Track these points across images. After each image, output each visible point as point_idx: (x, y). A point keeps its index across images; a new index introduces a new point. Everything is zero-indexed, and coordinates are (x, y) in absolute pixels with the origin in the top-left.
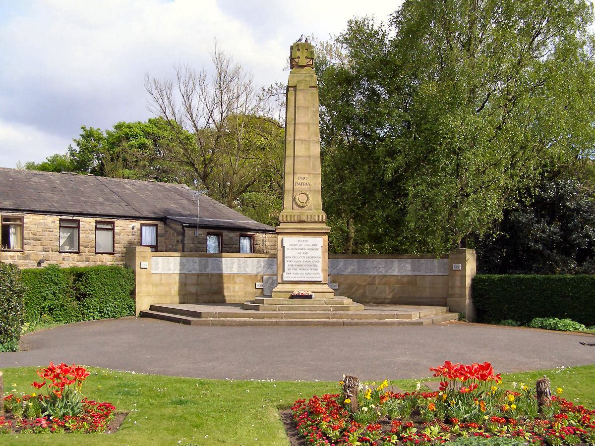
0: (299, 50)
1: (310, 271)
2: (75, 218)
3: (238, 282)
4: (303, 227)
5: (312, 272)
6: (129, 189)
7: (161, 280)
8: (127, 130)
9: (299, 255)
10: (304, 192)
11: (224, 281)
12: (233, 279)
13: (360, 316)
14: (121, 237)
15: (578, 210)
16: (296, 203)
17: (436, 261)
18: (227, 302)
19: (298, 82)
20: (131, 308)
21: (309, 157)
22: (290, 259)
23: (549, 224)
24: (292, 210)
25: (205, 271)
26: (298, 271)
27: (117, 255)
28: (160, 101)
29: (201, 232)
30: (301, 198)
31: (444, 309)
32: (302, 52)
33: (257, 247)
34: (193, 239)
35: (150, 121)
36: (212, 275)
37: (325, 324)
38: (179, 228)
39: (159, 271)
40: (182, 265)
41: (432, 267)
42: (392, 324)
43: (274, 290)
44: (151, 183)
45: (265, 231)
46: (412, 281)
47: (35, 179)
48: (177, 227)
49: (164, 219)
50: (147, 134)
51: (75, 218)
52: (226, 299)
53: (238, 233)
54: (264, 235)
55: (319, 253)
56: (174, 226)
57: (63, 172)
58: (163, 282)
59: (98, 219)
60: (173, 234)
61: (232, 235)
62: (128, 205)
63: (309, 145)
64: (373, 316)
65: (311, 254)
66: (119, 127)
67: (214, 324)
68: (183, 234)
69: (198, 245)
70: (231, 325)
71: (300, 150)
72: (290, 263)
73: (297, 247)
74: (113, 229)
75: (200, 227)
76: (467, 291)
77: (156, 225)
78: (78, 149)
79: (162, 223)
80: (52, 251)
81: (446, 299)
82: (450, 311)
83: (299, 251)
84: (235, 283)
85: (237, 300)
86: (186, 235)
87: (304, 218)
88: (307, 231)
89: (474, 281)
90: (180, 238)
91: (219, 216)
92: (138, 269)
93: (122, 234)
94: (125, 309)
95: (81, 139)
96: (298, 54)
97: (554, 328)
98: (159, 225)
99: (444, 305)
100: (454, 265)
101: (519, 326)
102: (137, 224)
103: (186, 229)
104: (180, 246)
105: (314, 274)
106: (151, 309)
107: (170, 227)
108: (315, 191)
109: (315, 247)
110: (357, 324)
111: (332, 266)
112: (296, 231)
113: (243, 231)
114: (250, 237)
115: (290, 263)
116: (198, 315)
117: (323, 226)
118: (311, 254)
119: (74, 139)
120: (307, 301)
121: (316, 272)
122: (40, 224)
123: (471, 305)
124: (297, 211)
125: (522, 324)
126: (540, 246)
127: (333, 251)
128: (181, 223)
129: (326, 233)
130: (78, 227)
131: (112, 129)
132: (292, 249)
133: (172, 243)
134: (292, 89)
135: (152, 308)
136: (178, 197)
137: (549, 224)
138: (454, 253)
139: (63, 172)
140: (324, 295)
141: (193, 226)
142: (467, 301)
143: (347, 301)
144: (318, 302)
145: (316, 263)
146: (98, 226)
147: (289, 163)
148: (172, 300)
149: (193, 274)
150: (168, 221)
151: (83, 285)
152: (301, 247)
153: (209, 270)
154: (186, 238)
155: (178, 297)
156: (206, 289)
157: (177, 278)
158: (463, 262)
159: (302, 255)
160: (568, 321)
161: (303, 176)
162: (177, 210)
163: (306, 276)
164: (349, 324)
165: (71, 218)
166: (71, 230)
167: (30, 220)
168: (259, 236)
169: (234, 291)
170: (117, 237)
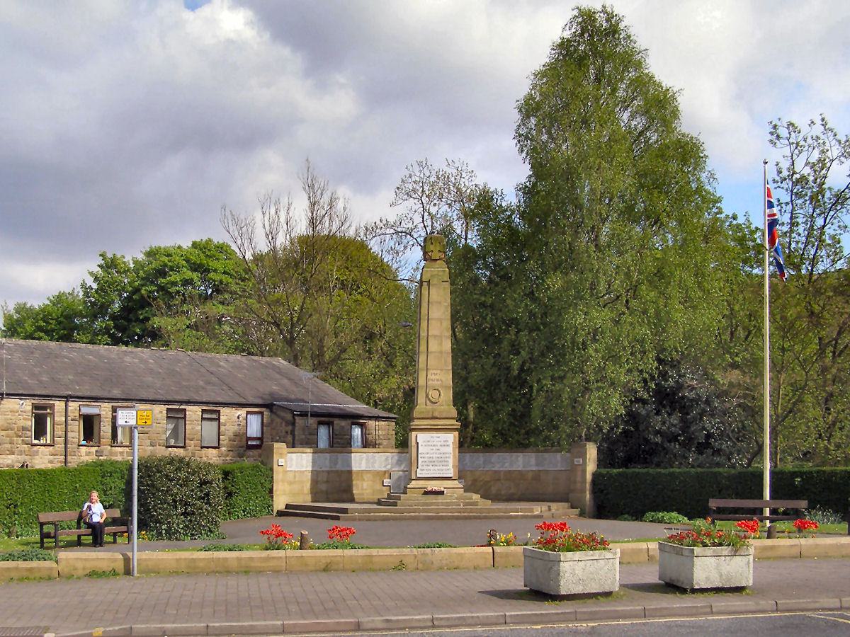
0: (432, 243)
2: (182, 407)
3: (366, 479)
4: (435, 423)
5: (443, 468)
6: (223, 367)
7: (295, 478)
8: (166, 259)
9: (432, 452)
10: (436, 388)
11: (353, 478)
12: (362, 476)
13: (489, 511)
14: (227, 427)
15: (697, 400)
16: (429, 399)
17: (558, 456)
18: (356, 500)
19: (431, 276)
20: (270, 506)
21: (441, 352)
22: (423, 455)
23: (670, 415)
24: (425, 406)
26: (431, 467)
27: (223, 449)
28: (239, 242)
29: (312, 421)
30: (433, 394)
31: (566, 505)
32: (435, 246)
33: (370, 437)
34: (303, 430)
35: (195, 245)
37: (457, 518)
38: (289, 417)
40: (314, 462)
41: (555, 462)
42: (516, 517)
43: (408, 486)
44: (244, 358)
45: (377, 418)
46: (537, 476)
47: (128, 359)
48: (286, 415)
49: (269, 406)
50: (195, 267)
51: (182, 407)
52: (355, 497)
53: (349, 422)
54: (377, 423)
56: (282, 414)
57: (152, 348)
58: (297, 479)
59: (204, 408)
61: (343, 423)
62: (231, 389)
63: (442, 340)
64: (499, 511)
66: (151, 254)
67: (360, 520)
68: (293, 424)
69: (309, 437)
70: (375, 519)
71: (433, 346)
73: (429, 444)
74: (219, 419)
75: (312, 416)
76: (588, 486)
77: (262, 413)
78: (95, 286)
79: (268, 410)
80: (159, 445)
81: (568, 494)
82: (572, 507)
83: (432, 447)
84: (364, 480)
85: (367, 497)
86: (297, 425)
87: (436, 414)
88: (439, 427)
89: (595, 475)
90: (290, 428)
91: (325, 399)
92: (275, 467)
93: (228, 425)
94: (265, 508)
95: (101, 272)
96: (432, 247)
97: (661, 521)
98: (265, 413)
99: (566, 501)
100: (575, 460)
101: (634, 520)
102: (242, 412)
103: (296, 417)
104: (290, 438)
106: (286, 508)
107: (278, 416)
108: (446, 387)
110: (485, 517)
111: (460, 460)
112: (429, 427)
113: (355, 418)
114: (362, 426)
116: (345, 511)
117: (454, 422)
119: (91, 271)
120: (440, 496)
123: (592, 502)
124: (430, 406)
125: (636, 520)
126: (658, 439)
127: (462, 445)
128: (292, 411)
129: (456, 430)
130: (185, 418)
131: (141, 257)
132: (425, 446)
133: (280, 434)
134: (426, 283)
135: (287, 506)
136: (278, 376)
137: (670, 415)
138: (576, 444)
139: (152, 348)
140: (454, 489)
141: (304, 414)
142: (588, 496)
143: (476, 497)
144: (449, 498)
145: (448, 459)
146: (205, 416)
147: (422, 358)
148: (305, 499)
149: (323, 471)
150: (274, 407)
151: (230, 483)
153: (339, 467)
154: (297, 428)
155: (310, 496)
156: (334, 488)
157: (309, 475)
158: (584, 455)
160: (674, 514)
161: (435, 372)
162: (281, 393)
164: (479, 518)
165: (177, 407)
166: (176, 420)
168: (371, 423)
169: (363, 488)
170: (222, 428)
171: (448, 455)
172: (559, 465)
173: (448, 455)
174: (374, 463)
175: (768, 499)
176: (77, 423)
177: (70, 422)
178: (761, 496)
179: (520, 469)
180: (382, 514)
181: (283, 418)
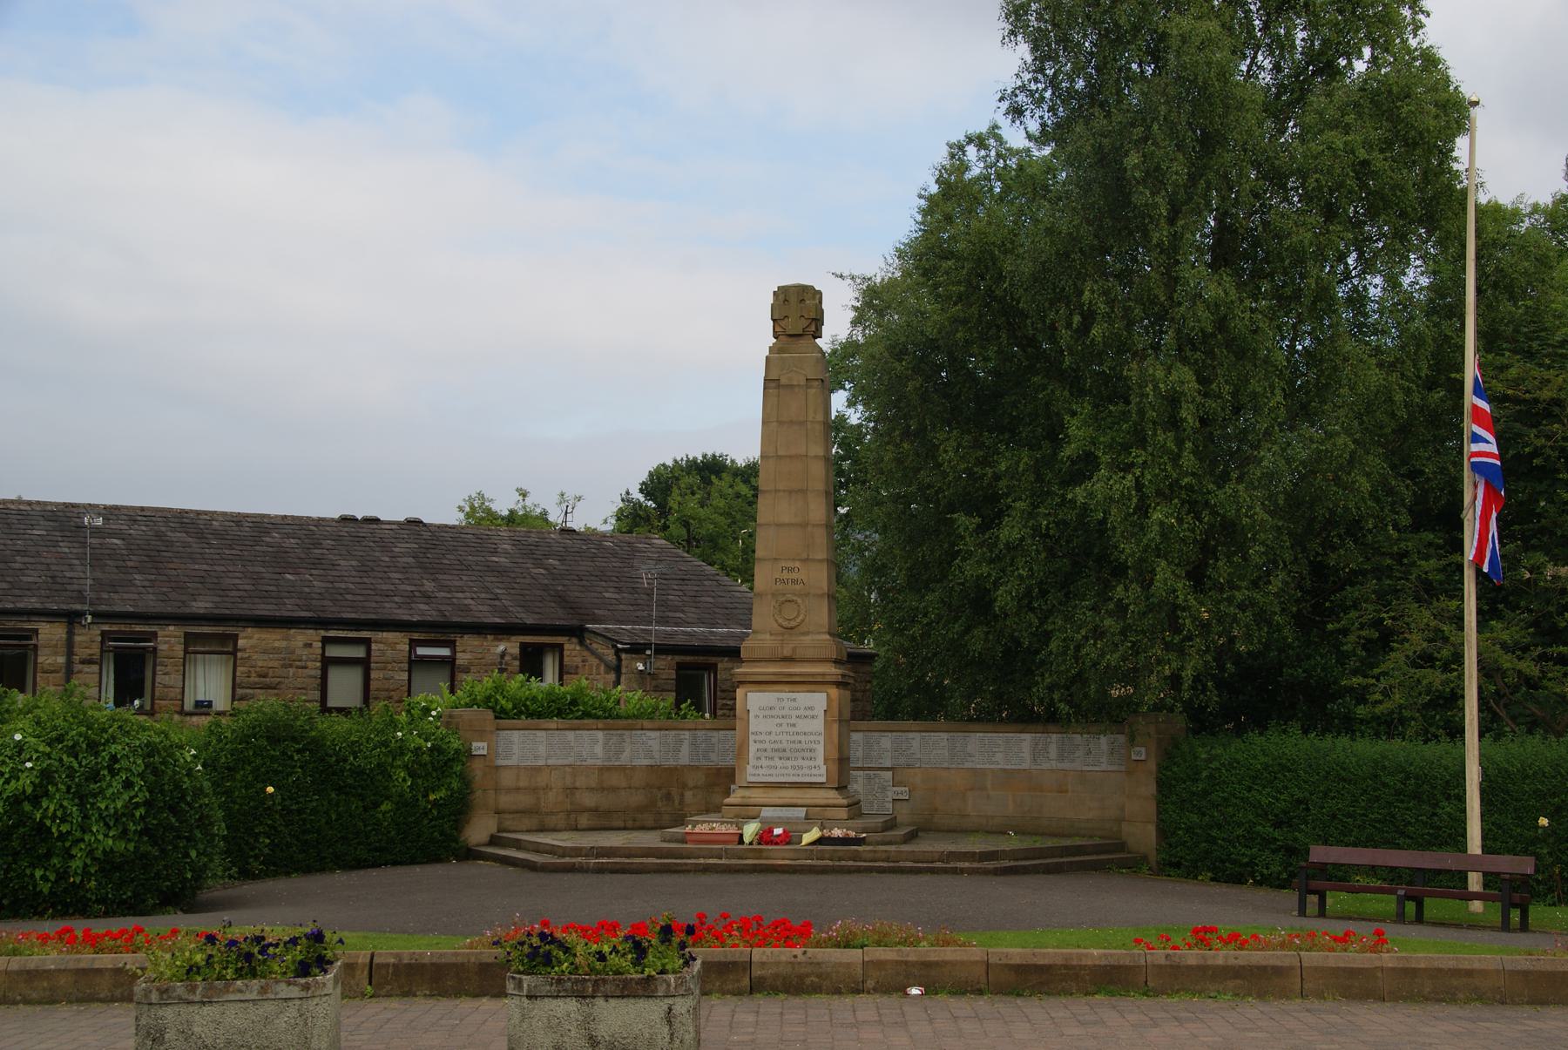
1: (800, 762)
5: (806, 763)
22: (758, 738)
25: (618, 759)
26: (779, 763)
36: (634, 768)
38: (610, 656)
39: (513, 761)
55: (818, 725)
60: (598, 667)
65: (803, 725)
72: (759, 746)
73: (773, 713)
83: (778, 721)
103: (623, 656)
105: (810, 768)
107: (593, 653)
109: (809, 713)
115: (759, 746)
118: (803, 725)
121: (812, 763)
122: (276, 651)
152: (781, 713)
159: (785, 728)
163: (792, 772)
167: (253, 642)
171: (812, 738)
172: (1104, 759)
173: (812, 738)
174: (620, 752)
175: (1479, 851)
176: (95, 668)
177: (77, 667)
178: (1457, 838)
179: (1025, 766)
180: (702, 861)
181: (600, 658)
